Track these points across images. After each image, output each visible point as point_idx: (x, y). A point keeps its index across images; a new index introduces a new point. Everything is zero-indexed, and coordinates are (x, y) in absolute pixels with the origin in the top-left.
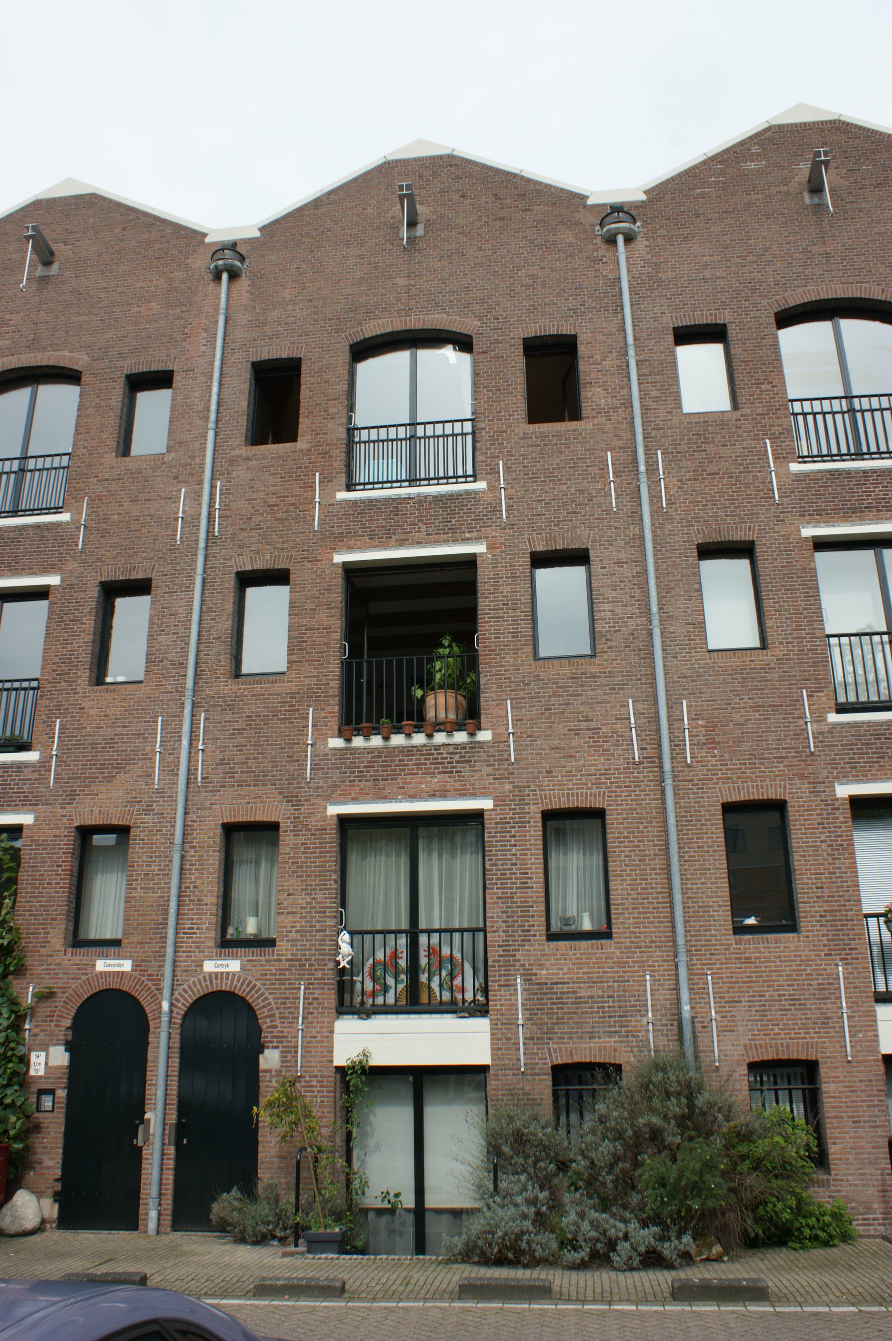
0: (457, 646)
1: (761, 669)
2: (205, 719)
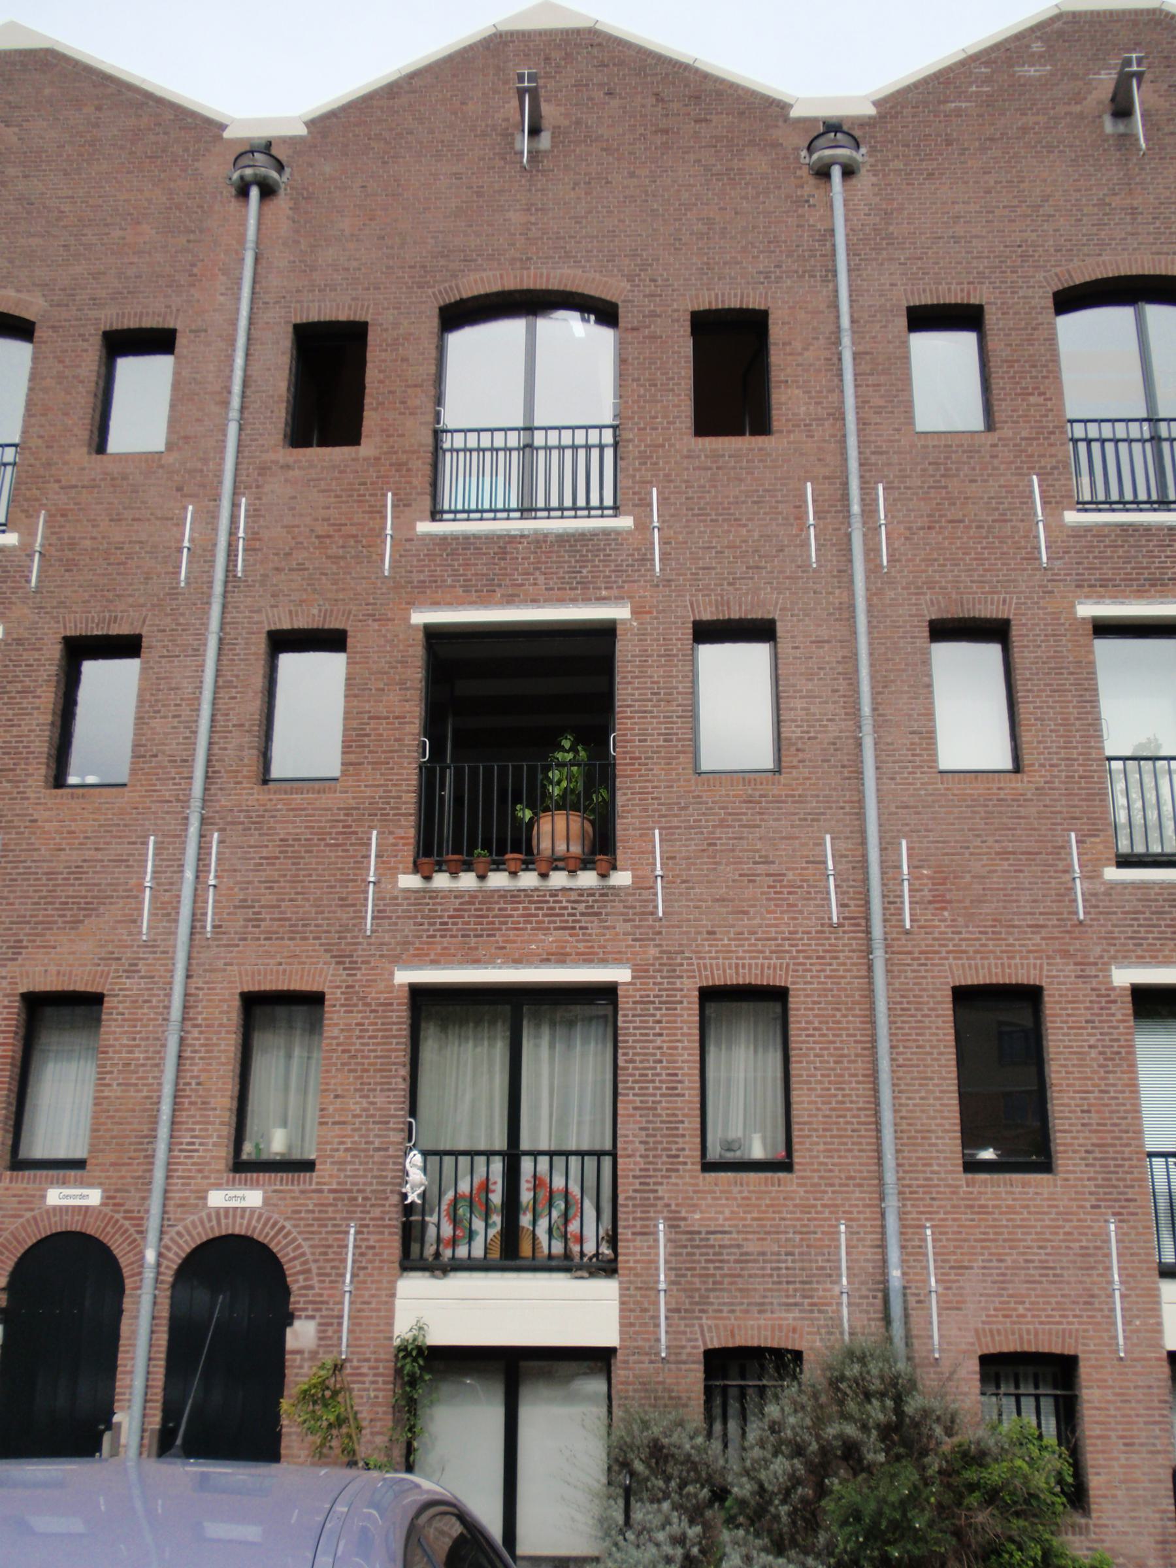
0: (584, 750)
1: (1013, 800)
2: (220, 842)
